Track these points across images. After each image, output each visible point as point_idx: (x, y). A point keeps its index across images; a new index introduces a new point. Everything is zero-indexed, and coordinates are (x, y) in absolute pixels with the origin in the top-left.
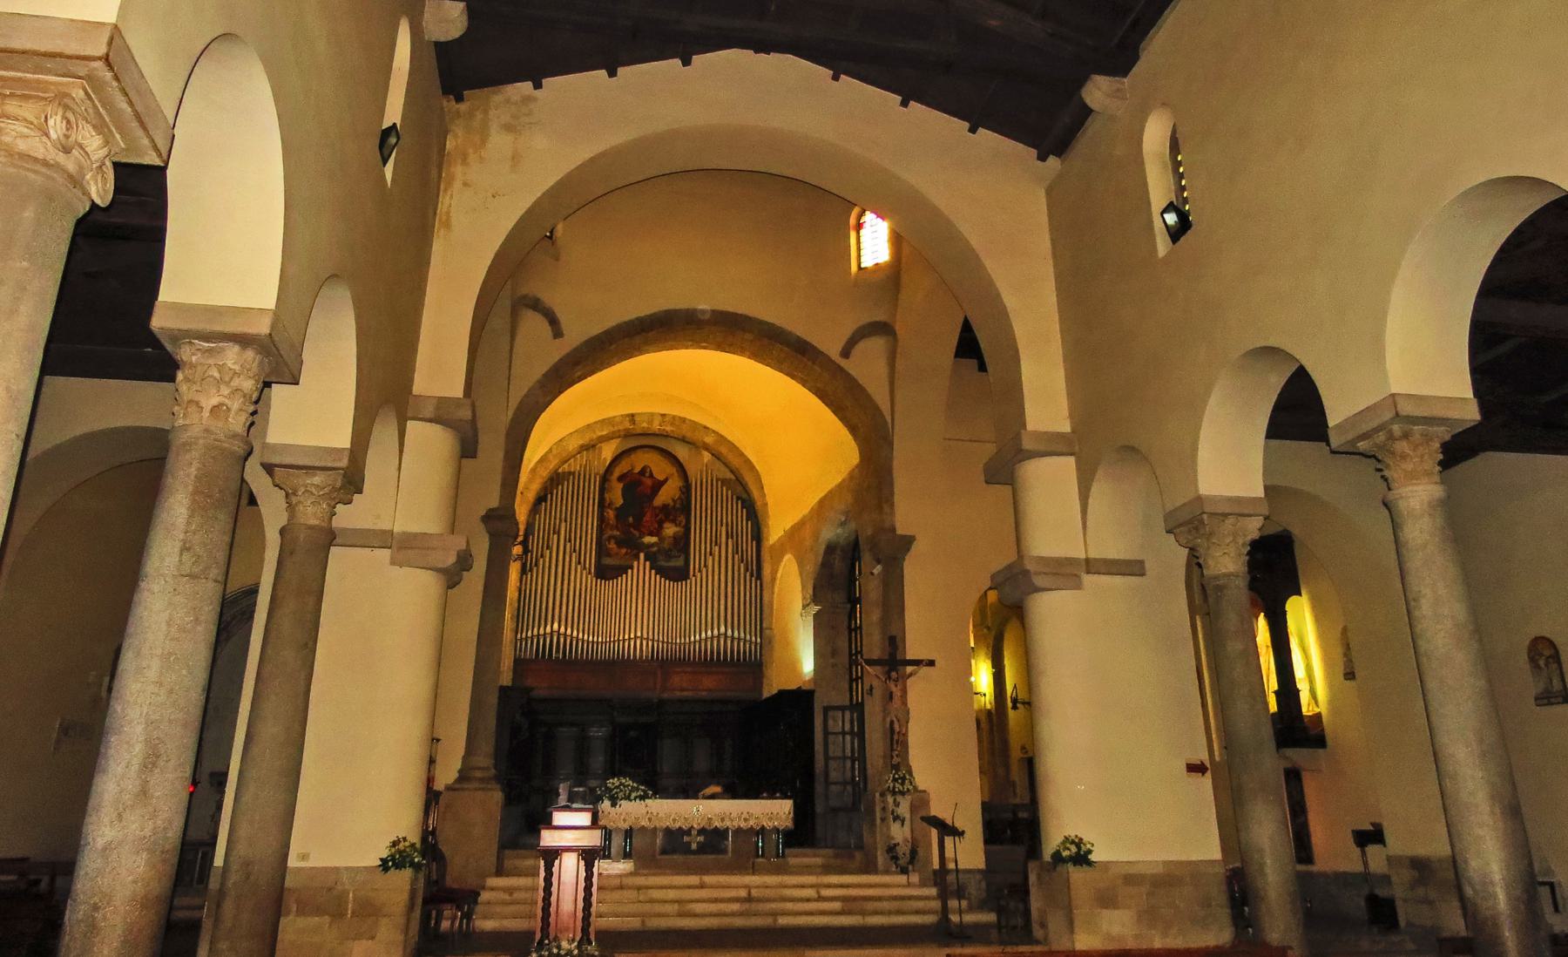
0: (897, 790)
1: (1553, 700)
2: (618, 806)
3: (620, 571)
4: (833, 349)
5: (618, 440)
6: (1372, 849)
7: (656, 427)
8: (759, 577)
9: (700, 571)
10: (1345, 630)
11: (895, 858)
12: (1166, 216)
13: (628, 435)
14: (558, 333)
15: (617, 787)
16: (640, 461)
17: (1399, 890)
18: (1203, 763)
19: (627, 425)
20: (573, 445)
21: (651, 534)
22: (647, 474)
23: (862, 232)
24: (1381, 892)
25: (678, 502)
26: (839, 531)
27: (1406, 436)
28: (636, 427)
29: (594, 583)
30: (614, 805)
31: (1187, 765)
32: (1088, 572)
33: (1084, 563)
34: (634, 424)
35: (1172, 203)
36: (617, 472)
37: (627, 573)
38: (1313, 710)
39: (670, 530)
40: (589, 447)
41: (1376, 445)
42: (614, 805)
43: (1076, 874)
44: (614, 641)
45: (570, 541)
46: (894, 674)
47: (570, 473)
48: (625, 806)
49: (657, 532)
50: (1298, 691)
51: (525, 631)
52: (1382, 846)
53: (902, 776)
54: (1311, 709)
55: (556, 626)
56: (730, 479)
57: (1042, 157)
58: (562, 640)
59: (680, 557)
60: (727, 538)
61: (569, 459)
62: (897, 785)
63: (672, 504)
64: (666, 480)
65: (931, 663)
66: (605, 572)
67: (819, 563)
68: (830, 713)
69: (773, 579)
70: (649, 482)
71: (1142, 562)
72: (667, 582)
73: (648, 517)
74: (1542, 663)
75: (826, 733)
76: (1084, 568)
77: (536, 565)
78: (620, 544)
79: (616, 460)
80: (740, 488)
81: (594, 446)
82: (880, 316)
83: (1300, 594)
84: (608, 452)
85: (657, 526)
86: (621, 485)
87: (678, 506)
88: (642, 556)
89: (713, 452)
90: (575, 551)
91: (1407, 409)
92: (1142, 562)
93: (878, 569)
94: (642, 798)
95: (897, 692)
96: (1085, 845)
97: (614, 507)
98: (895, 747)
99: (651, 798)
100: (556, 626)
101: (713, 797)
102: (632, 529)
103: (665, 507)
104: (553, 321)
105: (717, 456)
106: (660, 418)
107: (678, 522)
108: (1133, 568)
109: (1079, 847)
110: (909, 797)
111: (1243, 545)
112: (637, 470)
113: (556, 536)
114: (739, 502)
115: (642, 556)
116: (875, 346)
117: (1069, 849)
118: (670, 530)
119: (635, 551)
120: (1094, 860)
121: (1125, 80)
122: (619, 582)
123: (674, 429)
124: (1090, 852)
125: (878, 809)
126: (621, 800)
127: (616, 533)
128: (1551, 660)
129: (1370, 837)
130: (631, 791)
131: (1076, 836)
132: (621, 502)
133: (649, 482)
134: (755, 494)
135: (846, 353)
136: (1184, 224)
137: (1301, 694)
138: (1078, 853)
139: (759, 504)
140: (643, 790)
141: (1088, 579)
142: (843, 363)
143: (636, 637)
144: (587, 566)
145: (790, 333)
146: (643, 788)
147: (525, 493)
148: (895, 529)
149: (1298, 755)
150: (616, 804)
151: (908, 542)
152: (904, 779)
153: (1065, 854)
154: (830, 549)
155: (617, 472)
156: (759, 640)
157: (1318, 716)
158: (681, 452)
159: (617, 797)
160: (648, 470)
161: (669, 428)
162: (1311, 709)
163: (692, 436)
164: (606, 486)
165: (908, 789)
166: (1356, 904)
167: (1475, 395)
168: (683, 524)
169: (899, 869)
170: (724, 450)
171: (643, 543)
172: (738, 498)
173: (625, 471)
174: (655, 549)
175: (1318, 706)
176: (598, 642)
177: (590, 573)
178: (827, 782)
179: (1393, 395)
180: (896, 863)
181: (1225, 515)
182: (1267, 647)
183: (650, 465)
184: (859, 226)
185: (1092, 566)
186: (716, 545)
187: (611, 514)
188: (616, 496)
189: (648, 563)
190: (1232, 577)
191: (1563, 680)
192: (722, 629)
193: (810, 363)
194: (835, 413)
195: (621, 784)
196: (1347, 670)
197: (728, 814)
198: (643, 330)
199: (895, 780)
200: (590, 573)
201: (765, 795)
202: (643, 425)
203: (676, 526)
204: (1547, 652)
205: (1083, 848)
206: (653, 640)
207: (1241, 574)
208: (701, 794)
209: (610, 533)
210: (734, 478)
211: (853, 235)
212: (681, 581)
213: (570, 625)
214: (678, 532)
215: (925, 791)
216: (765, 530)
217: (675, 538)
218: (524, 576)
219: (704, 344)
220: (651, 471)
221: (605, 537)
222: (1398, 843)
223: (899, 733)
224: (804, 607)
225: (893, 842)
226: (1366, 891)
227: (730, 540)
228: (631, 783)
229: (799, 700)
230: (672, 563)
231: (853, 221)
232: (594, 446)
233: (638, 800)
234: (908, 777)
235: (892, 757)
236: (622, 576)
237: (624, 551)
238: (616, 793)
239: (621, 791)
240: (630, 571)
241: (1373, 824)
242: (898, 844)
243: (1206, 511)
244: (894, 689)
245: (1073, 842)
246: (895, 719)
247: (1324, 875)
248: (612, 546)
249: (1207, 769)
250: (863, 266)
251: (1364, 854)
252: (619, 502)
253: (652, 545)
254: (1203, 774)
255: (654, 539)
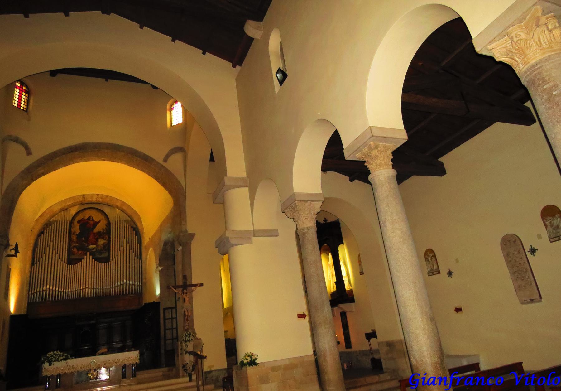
0: (187, 340)
1: (434, 273)
2: (52, 365)
3: (79, 260)
4: (160, 160)
5: (78, 206)
6: (372, 340)
7: (94, 200)
8: (141, 258)
9: (115, 258)
10: (359, 256)
11: (186, 370)
12: (278, 75)
13: (82, 204)
14: (29, 153)
15: (52, 356)
16: (87, 215)
17: (382, 355)
18: (304, 314)
19: (81, 199)
20: (57, 209)
21: (93, 244)
22: (91, 220)
23: (172, 112)
24: (376, 356)
25: (105, 230)
26: (169, 236)
27: (376, 147)
28: (85, 200)
29: (66, 267)
30: (50, 365)
31: (298, 315)
32: (254, 236)
33: (252, 232)
34: (84, 199)
35: (280, 69)
36: (77, 219)
37: (81, 261)
38: (350, 288)
39: (101, 242)
40: (65, 209)
41: (364, 154)
42: (50, 365)
43: (250, 370)
44: (76, 291)
45: (55, 249)
46: (185, 291)
47: (55, 221)
48: (56, 364)
49: (95, 243)
50: (344, 281)
51: (33, 289)
52: (376, 339)
53: (189, 333)
54: (349, 288)
55: (48, 287)
56: (129, 220)
57: (234, 66)
58: (51, 292)
59: (105, 253)
60: (127, 243)
61: (55, 215)
62: (187, 338)
63: (102, 231)
64: (99, 221)
65: (202, 285)
66: (70, 262)
67: (161, 250)
68: (167, 311)
69: (146, 259)
70: (92, 222)
71: (277, 230)
72: (98, 263)
73: (91, 238)
74: (429, 259)
75: (165, 319)
76: (253, 235)
77: (39, 261)
78: (78, 249)
79: (77, 214)
80: (132, 223)
81: (67, 209)
82: (179, 145)
83: (343, 244)
84: (73, 211)
85: (95, 241)
86: (79, 225)
87: (105, 232)
88: (88, 253)
89: (120, 209)
90: (57, 254)
91: (375, 133)
92: (277, 230)
93: (180, 248)
94: (65, 359)
95: (187, 299)
96: (254, 356)
97: (76, 234)
98: (186, 321)
99: (70, 359)
100: (48, 287)
101: (103, 354)
102: (84, 243)
103: (99, 233)
104: (27, 148)
105: (122, 210)
106: (96, 196)
107: (105, 239)
108: (273, 233)
109: (251, 358)
110: (192, 343)
111: (314, 215)
112: (86, 218)
113: (48, 248)
114: (132, 229)
115: (88, 253)
116: (177, 157)
117: (247, 359)
118: (101, 242)
119: (85, 252)
120: (258, 362)
121: (262, 23)
122: (78, 266)
123: (103, 200)
124: (256, 359)
125: (179, 348)
126: (54, 362)
127: (77, 245)
128: (432, 258)
129: (371, 335)
130: (59, 357)
131: (251, 353)
132: (79, 231)
133: (92, 222)
134: (138, 224)
135: (165, 160)
136: (285, 76)
137: (345, 282)
138: (251, 361)
139: (140, 228)
140: (65, 356)
141: (254, 239)
142: (165, 164)
143: (86, 288)
144: (63, 260)
145: (141, 152)
146: (66, 354)
147: (33, 230)
148: (187, 231)
149: (344, 307)
150: (51, 364)
151: (192, 236)
152: (190, 335)
153: (245, 361)
154: (166, 244)
155: (77, 219)
156: (141, 284)
157: (351, 291)
158: (107, 210)
159: (52, 360)
160: (92, 218)
161: (100, 200)
162: (349, 288)
163: (111, 203)
164: (72, 225)
165: (192, 339)
166: (367, 362)
167: (405, 128)
168: (107, 239)
169: (188, 374)
170: (125, 208)
171: (89, 248)
172: (131, 227)
173: (81, 219)
174: (94, 250)
175: (351, 286)
176: (68, 292)
177: (65, 262)
178: (165, 340)
179: (370, 127)
180: (186, 372)
181: (305, 201)
182: (332, 266)
183: (92, 216)
184: (171, 109)
185: (256, 233)
186: (122, 246)
187: (74, 237)
188: (77, 229)
189: (91, 256)
190: (309, 229)
191: (437, 265)
192: (125, 281)
193: (150, 165)
194: (163, 186)
195: (54, 354)
196: (360, 272)
197: (108, 361)
198: (72, 152)
199: (186, 336)
200: (65, 262)
201: (126, 350)
202: (88, 199)
203: (104, 240)
204: (431, 255)
205: (253, 358)
206: (94, 289)
207: (313, 227)
208: (97, 353)
209: (74, 245)
210: (130, 219)
211: (168, 113)
212: (105, 263)
213: (60, 287)
214: (105, 242)
215: (200, 339)
216: (143, 239)
217: (104, 245)
218: (33, 266)
219: (103, 158)
220: (93, 218)
221: (72, 246)
222: (382, 337)
223: (187, 315)
224: (156, 268)
225: (185, 363)
226: (371, 357)
227: (128, 245)
228: (59, 353)
229: (155, 306)
230: (103, 256)
231: (168, 107)
232: (67, 209)
233: (63, 361)
234: (192, 334)
235: (185, 326)
236: (79, 263)
237: (80, 252)
238: (52, 359)
239: (54, 357)
240: (83, 260)
241: (372, 330)
242: (188, 363)
243: (297, 199)
244: (185, 297)
245: (249, 356)
246: (186, 310)
247: (356, 352)
248: (75, 250)
249: (306, 316)
250: (173, 125)
251: (369, 342)
252: (78, 231)
253: (94, 249)
254: (304, 318)
255: (94, 246)
